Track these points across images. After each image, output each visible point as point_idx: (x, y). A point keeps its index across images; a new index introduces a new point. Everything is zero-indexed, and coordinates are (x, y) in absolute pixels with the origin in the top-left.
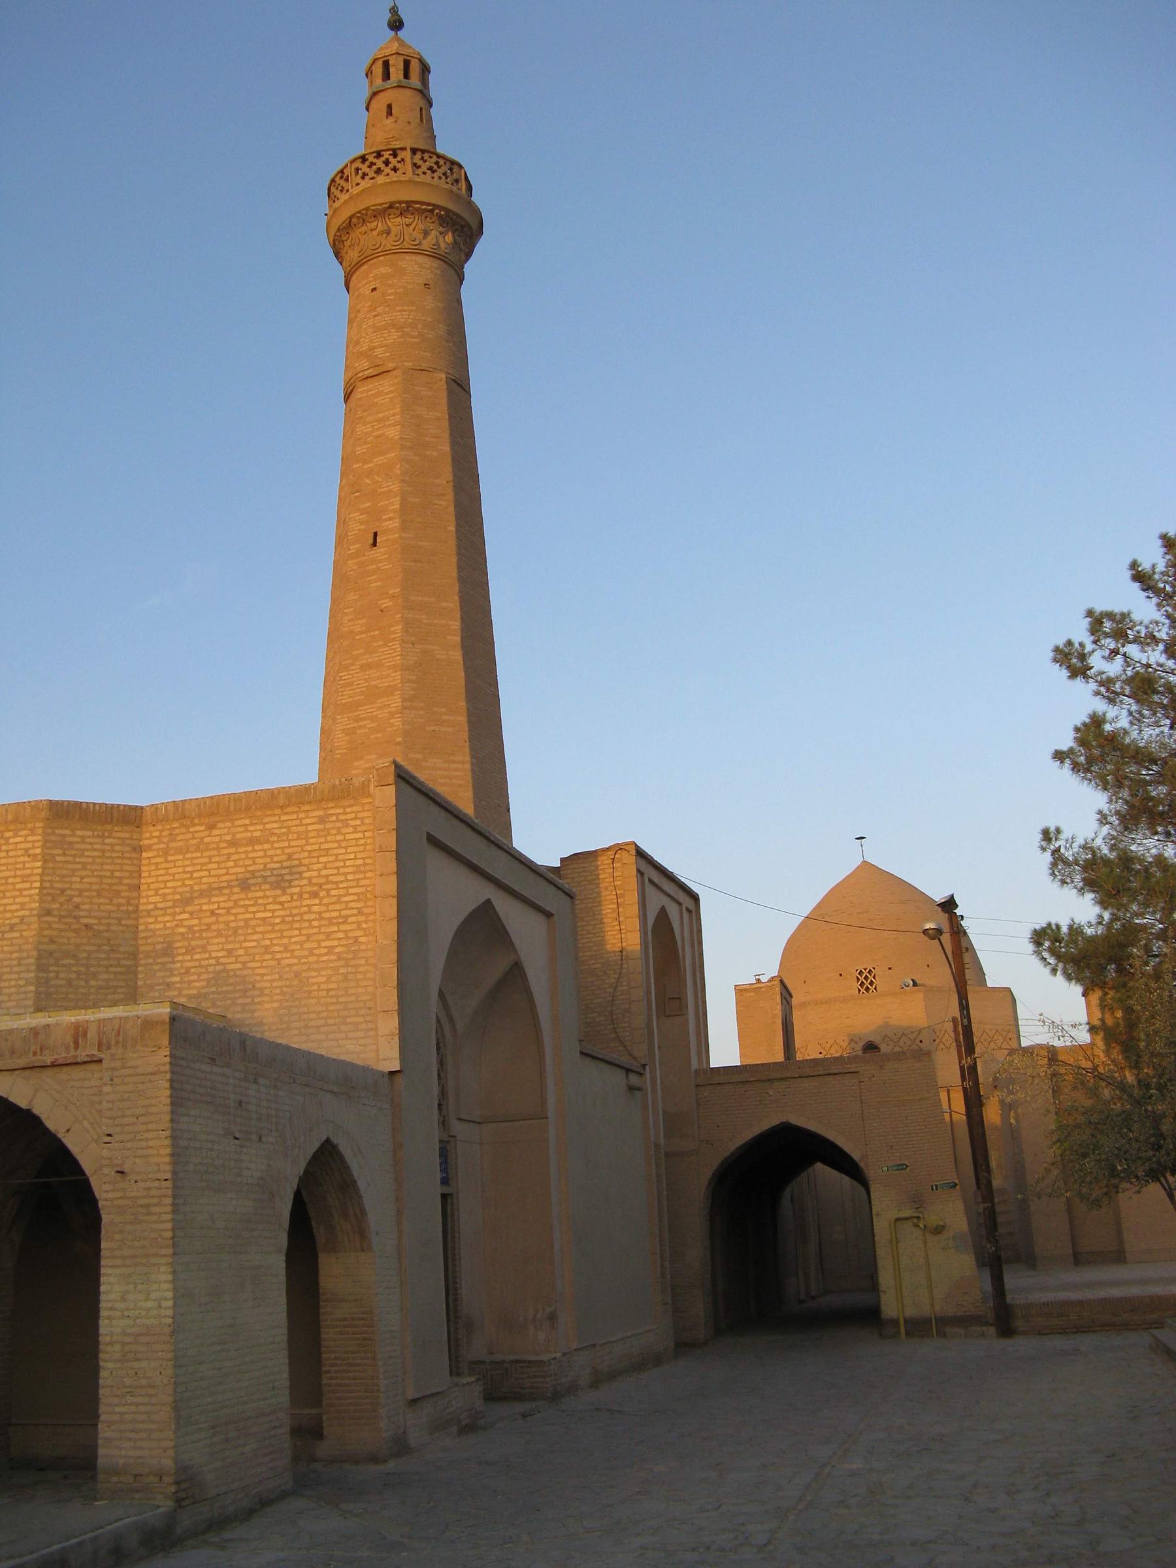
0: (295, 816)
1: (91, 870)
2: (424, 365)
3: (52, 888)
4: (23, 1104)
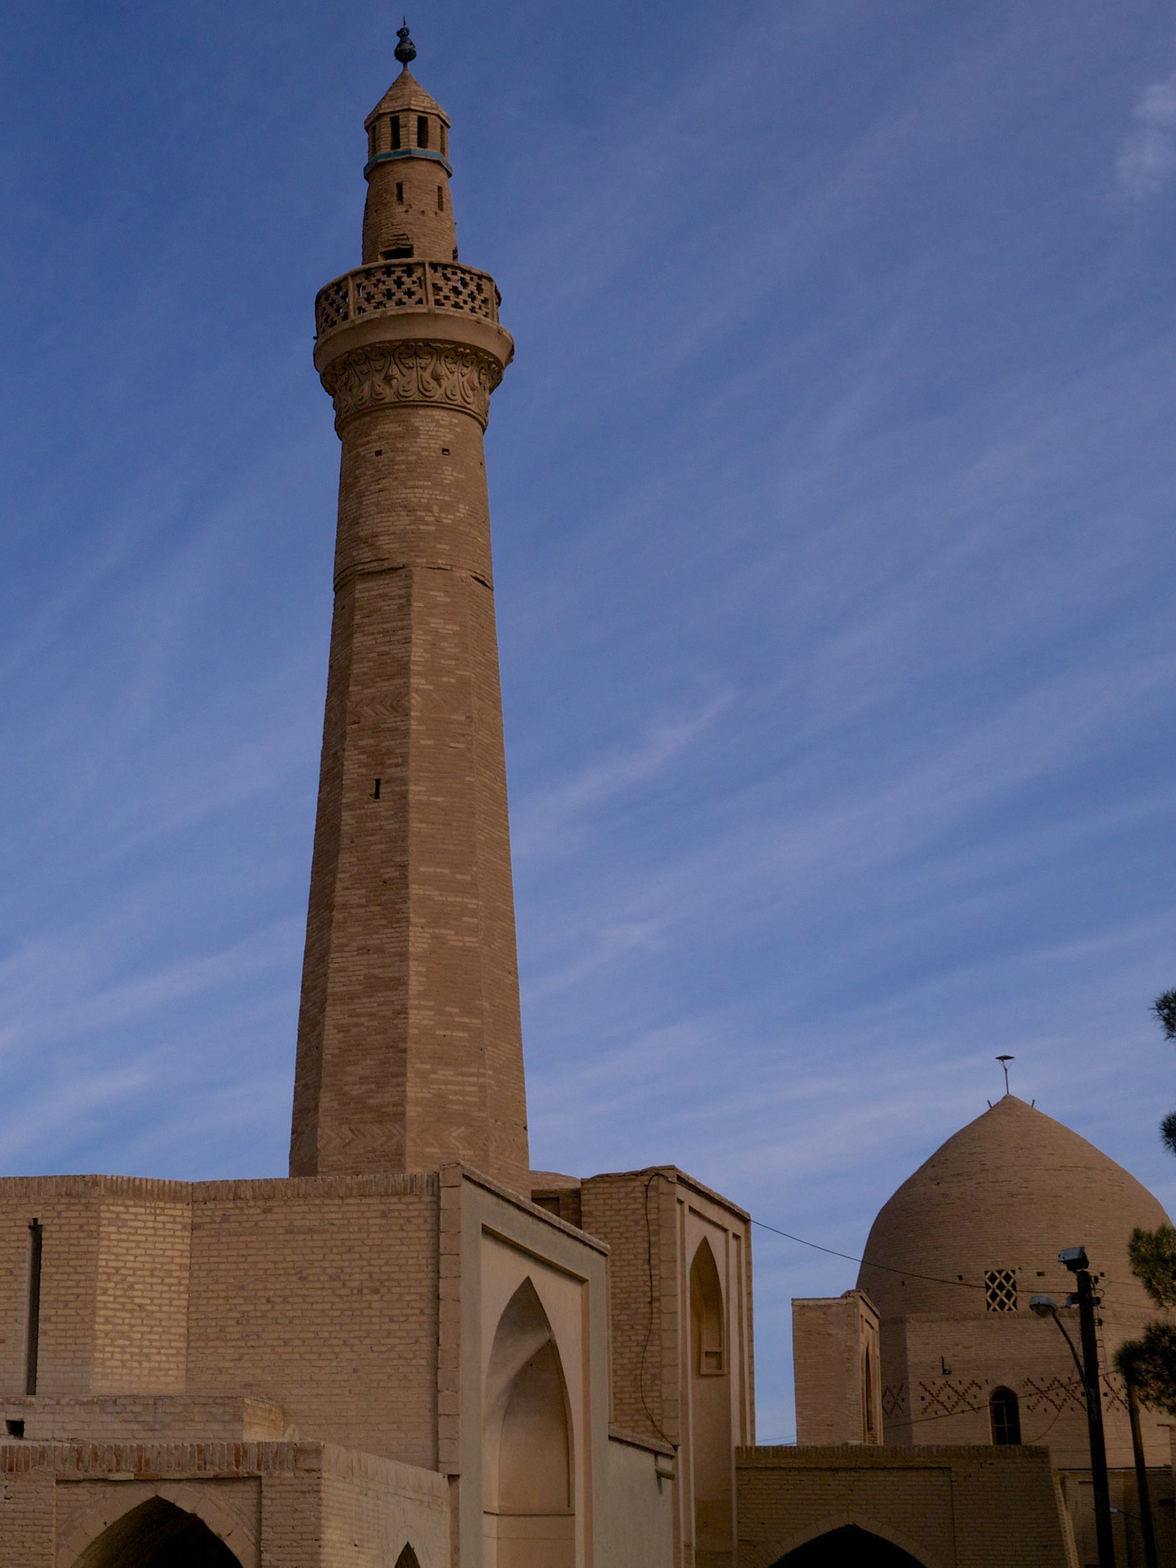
1: (144, 1249)
4: (188, 1508)
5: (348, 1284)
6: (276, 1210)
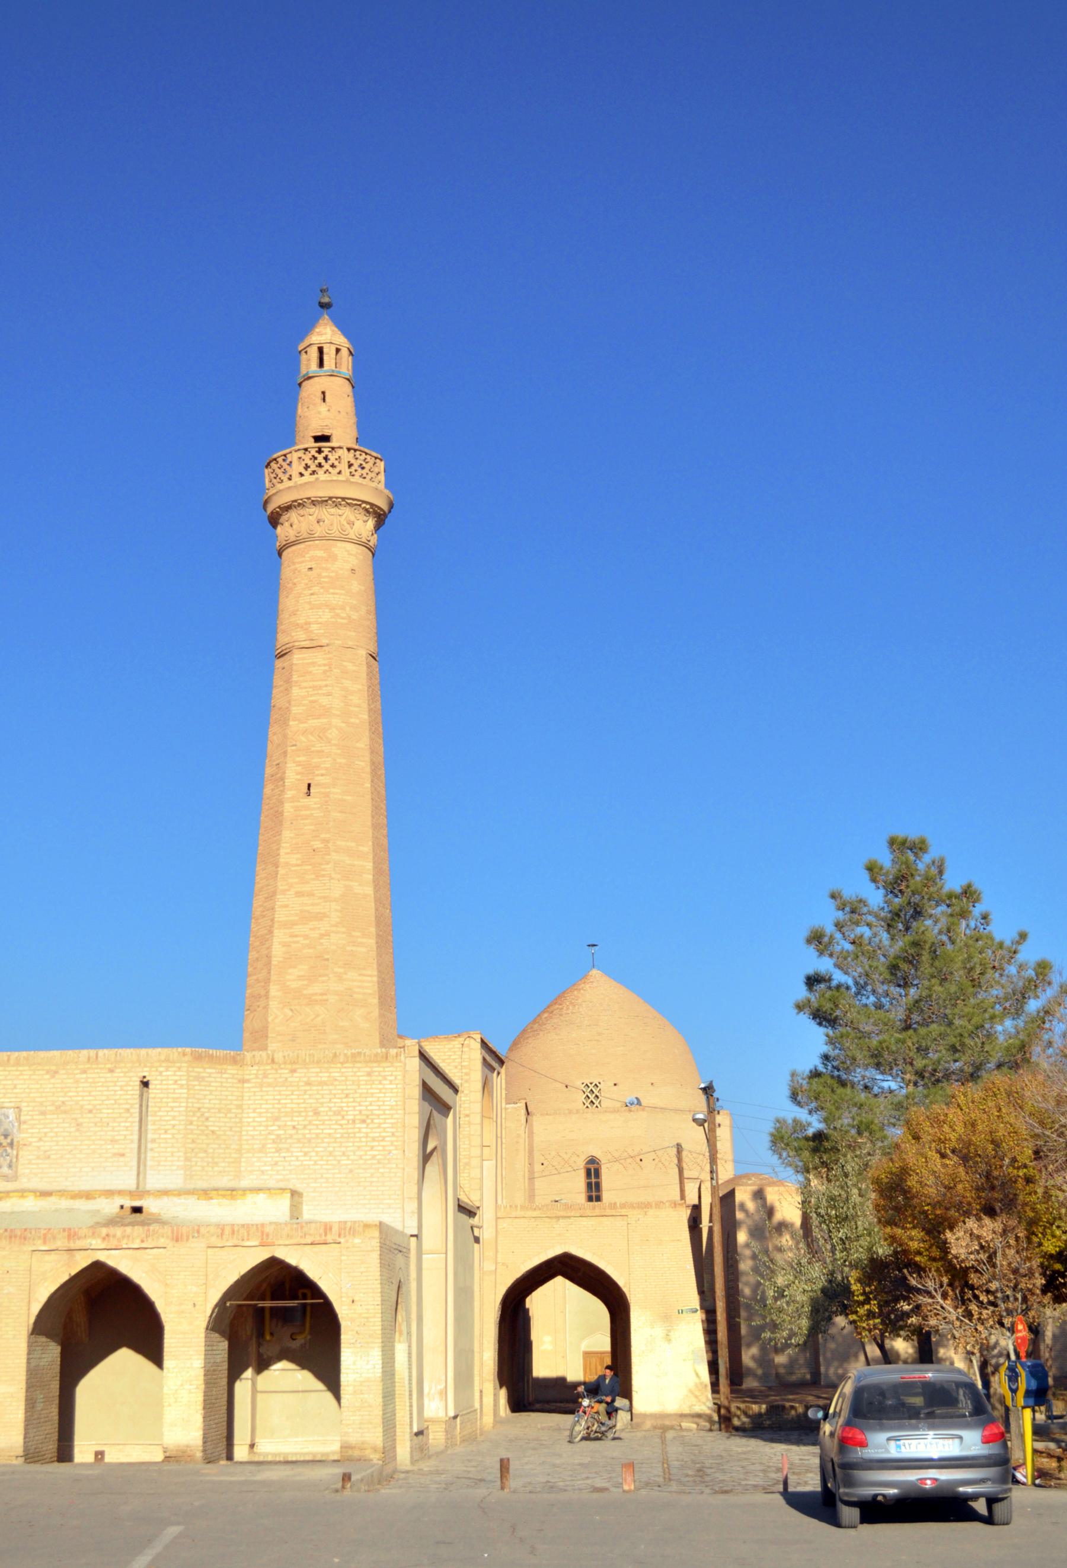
0: (350, 1070)
2: (350, 643)
3: (193, 1107)
5: (346, 1117)
6: (299, 1071)
